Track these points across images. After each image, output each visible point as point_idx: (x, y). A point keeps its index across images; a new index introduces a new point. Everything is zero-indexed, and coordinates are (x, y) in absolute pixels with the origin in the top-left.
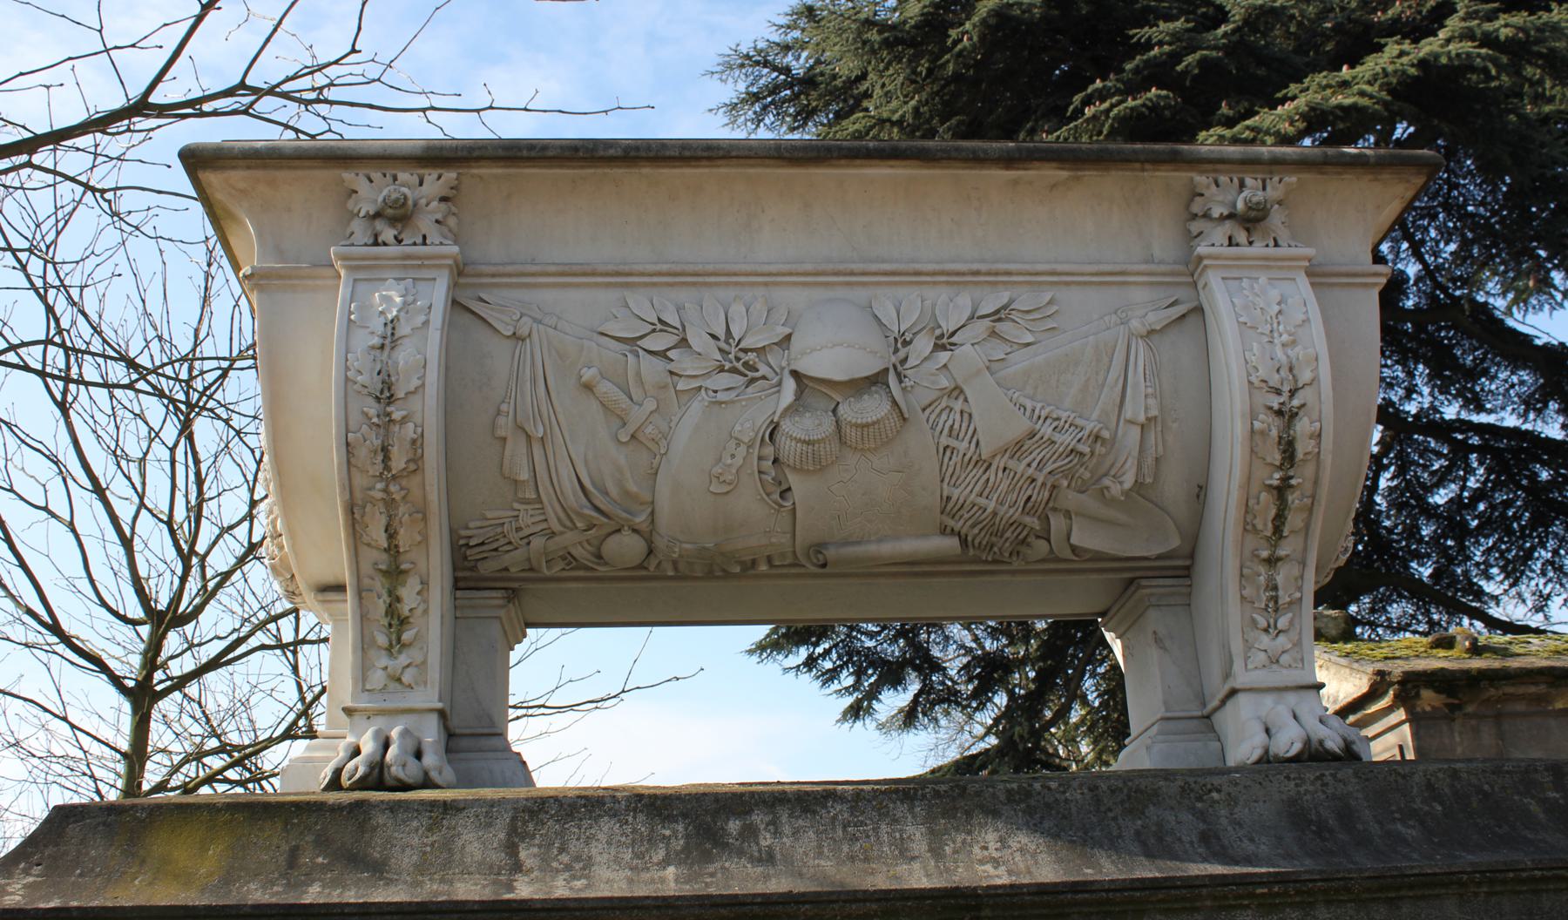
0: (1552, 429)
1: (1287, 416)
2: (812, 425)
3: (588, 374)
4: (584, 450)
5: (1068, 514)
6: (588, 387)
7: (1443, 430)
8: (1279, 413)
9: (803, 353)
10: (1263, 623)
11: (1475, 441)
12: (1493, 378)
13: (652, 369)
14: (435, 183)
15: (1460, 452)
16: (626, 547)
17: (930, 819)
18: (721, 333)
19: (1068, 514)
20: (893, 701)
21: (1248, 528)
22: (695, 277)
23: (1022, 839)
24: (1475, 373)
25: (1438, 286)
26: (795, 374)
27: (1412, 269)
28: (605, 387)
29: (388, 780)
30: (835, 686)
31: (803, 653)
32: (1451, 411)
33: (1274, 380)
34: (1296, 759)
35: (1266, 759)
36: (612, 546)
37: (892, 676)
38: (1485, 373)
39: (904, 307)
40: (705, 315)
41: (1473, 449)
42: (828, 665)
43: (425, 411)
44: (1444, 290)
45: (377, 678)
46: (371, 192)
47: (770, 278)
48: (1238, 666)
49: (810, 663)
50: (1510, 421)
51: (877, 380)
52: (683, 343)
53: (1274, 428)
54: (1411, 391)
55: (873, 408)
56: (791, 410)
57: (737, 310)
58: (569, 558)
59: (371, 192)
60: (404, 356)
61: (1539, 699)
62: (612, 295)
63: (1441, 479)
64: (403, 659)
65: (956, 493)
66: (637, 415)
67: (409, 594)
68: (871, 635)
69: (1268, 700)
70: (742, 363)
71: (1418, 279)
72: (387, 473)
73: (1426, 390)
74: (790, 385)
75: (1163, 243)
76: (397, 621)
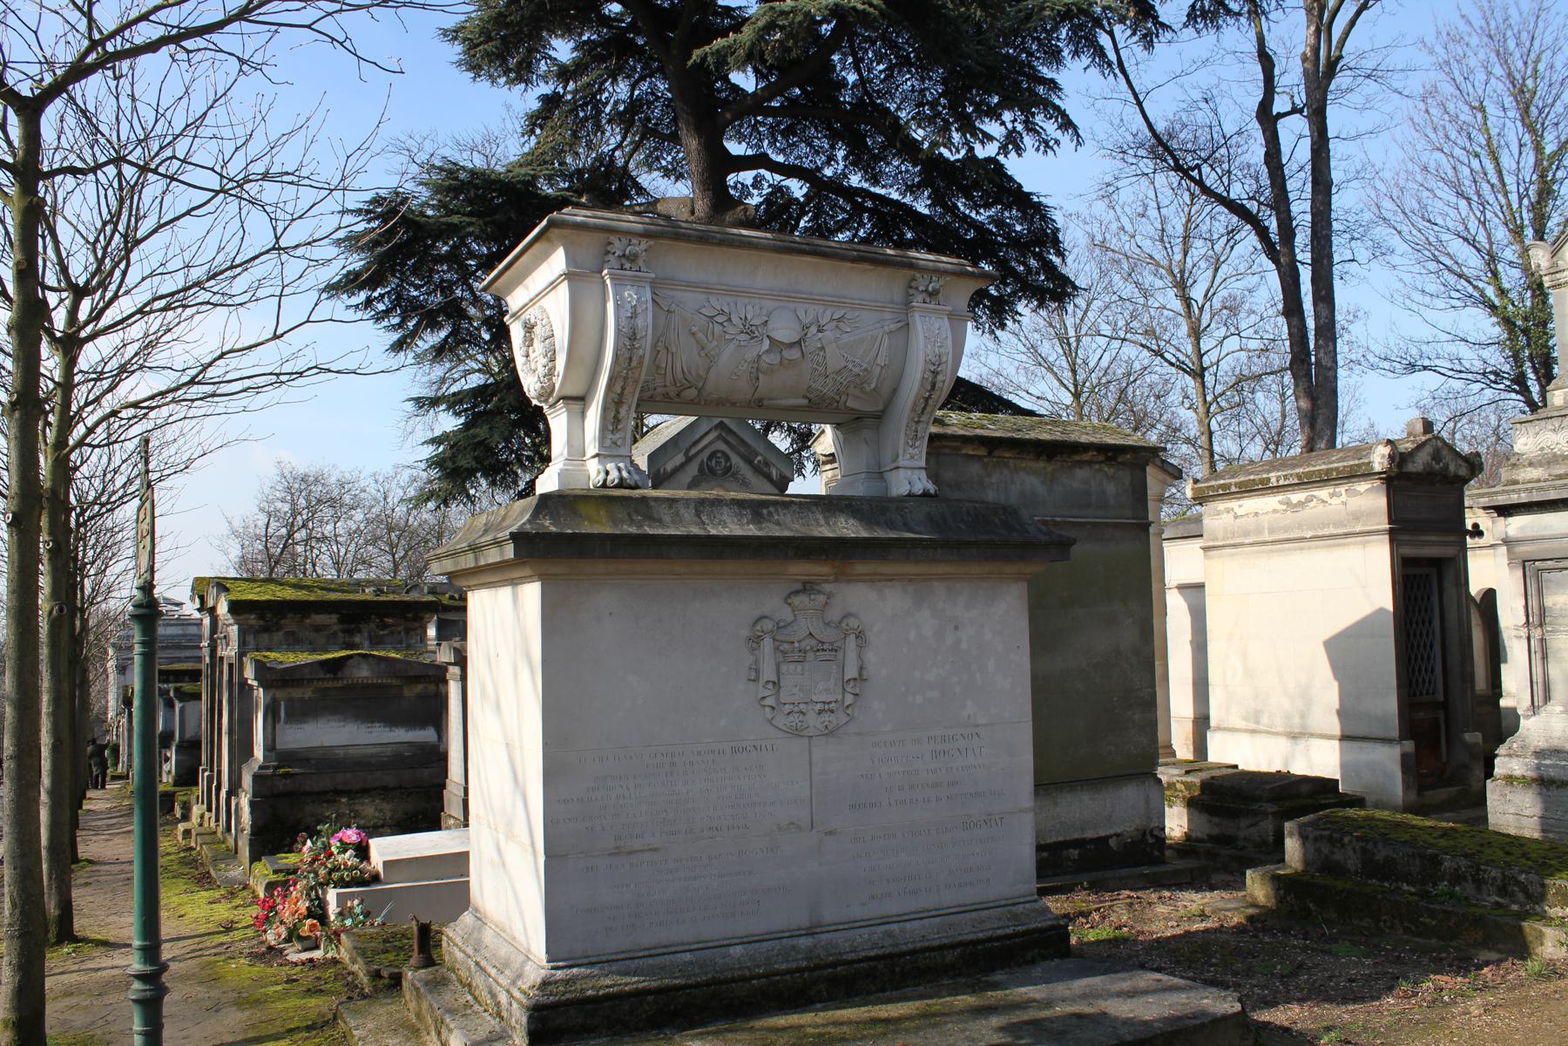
0: (922, 207)
1: (935, 373)
2: (773, 359)
3: (694, 329)
4: (686, 357)
7: (850, 193)
11: (869, 204)
12: (888, 164)
13: (718, 328)
14: (644, 244)
15: (858, 210)
16: (692, 393)
17: (823, 513)
20: (431, 339)
21: (914, 410)
23: (851, 521)
24: (877, 158)
25: (866, 92)
27: (852, 78)
28: (700, 335)
30: (385, 323)
31: (362, 296)
32: (855, 180)
35: (910, 495)
37: (430, 320)
38: (884, 159)
39: (809, 313)
41: (867, 210)
42: (381, 307)
43: (646, 345)
44: (870, 97)
45: (608, 442)
49: (368, 303)
50: (895, 196)
51: (798, 343)
54: (831, 159)
55: (794, 354)
56: (766, 352)
58: (666, 395)
60: (640, 322)
61: (955, 448)
62: (703, 297)
63: (842, 226)
67: (623, 411)
68: (417, 288)
69: (909, 472)
70: (749, 331)
71: (854, 85)
72: (629, 368)
73: (842, 164)
74: (767, 342)
75: (898, 294)
76: (617, 420)
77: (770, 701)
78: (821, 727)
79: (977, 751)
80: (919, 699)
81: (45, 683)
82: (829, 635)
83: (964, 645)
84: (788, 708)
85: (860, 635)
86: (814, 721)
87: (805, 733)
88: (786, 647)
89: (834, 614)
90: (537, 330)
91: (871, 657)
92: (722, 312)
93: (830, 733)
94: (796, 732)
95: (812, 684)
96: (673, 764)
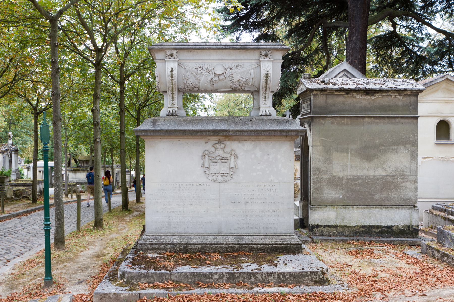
2: (216, 79)
3: (192, 72)
6: (192, 74)
13: (199, 72)
22: (204, 61)
36: (195, 89)
39: (227, 65)
46: (169, 53)
47: (213, 61)
52: (202, 69)
55: (222, 77)
57: (208, 65)
59: (169, 53)
66: (198, 76)
70: (209, 71)
74: (214, 74)
79: (274, 190)
82: (226, 155)
83: (271, 159)
86: (220, 178)
88: (212, 158)
92: (200, 67)
93: (225, 181)
94: (215, 181)
95: (222, 168)
96: (180, 187)
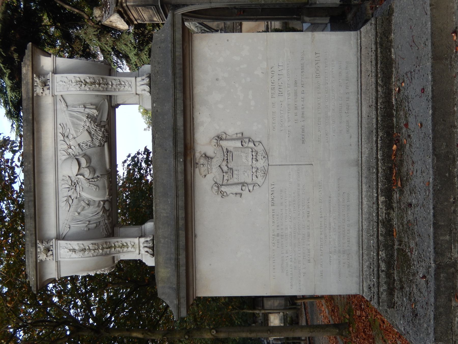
5: (101, 122)
8: (86, 85)
9: (73, 174)
10: (123, 87)
18: (68, 189)
19: (101, 122)
26: (76, 175)
29: (152, 246)
33: (79, 85)
34: (150, 87)
35: (150, 92)
40: (64, 193)
48: (131, 92)
51: (77, 160)
53: (88, 86)
56: (84, 177)
57: (64, 186)
60: (77, 248)
64: (129, 245)
65: (97, 144)
70: (74, 185)
74: (79, 176)
77: (251, 187)
78: (264, 160)
79: (281, 68)
80: (253, 103)
81: (280, 17)
84: (254, 178)
85: (219, 138)
86: (261, 163)
87: (266, 168)
89: (210, 151)
90: (97, 205)
91: (231, 131)
93: (267, 155)
94: (266, 173)
95: (243, 161)
96: (278, 235)
